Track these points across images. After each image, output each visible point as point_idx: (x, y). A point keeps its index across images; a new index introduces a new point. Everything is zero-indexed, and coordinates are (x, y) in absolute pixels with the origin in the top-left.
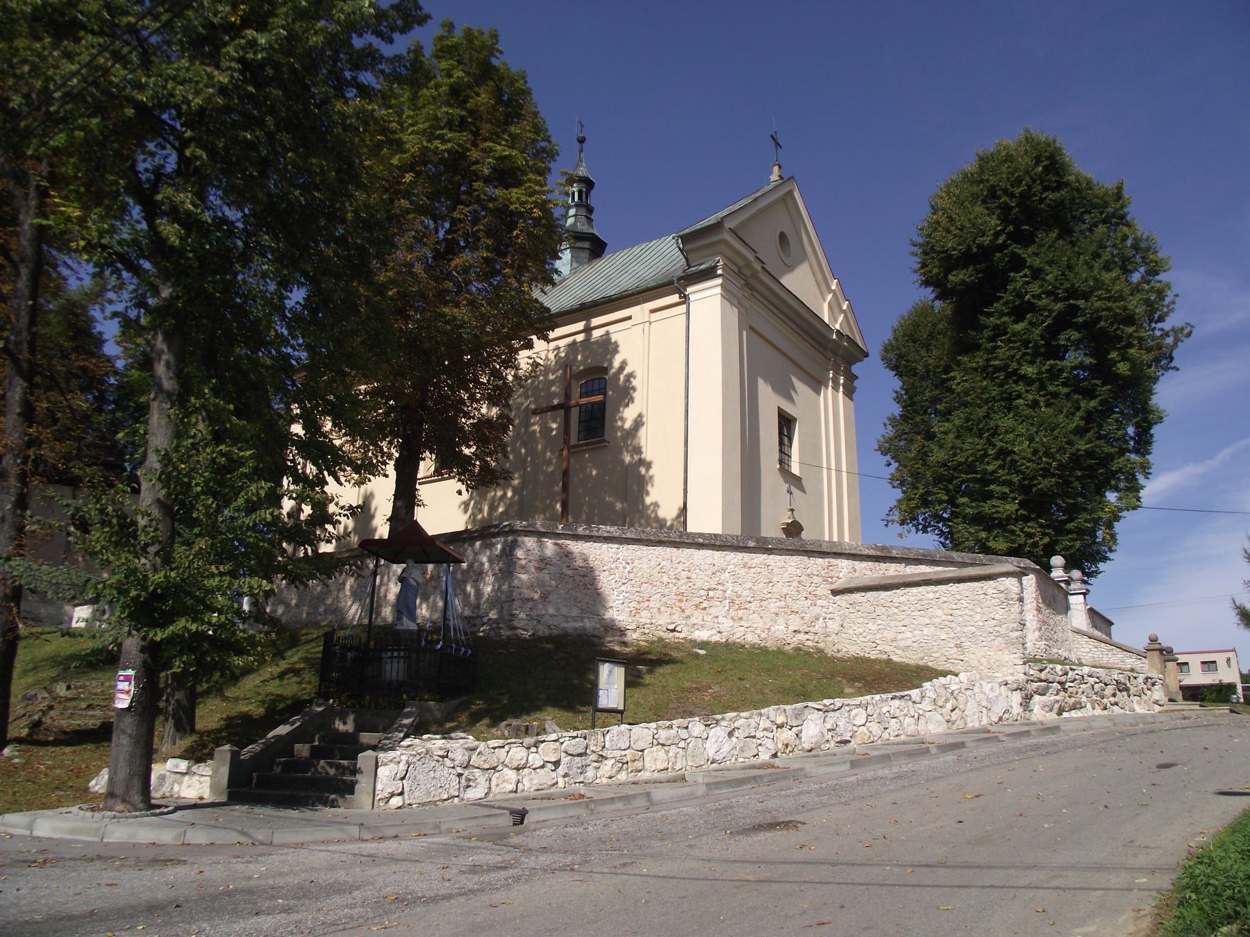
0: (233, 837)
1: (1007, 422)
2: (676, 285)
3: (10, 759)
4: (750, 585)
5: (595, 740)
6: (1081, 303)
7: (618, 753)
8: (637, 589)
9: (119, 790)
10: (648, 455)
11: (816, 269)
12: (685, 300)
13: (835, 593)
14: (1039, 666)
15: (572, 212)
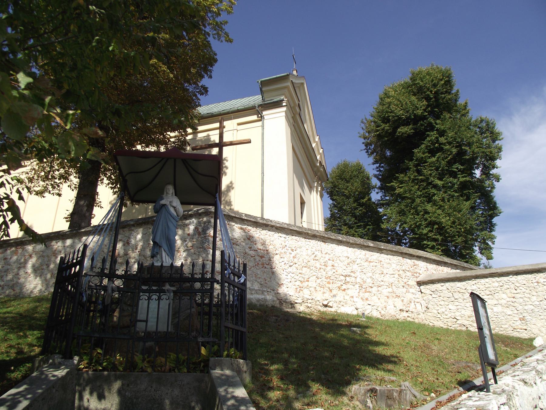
2: (257, 110)
4: (371, 274)
12: (261, 118)
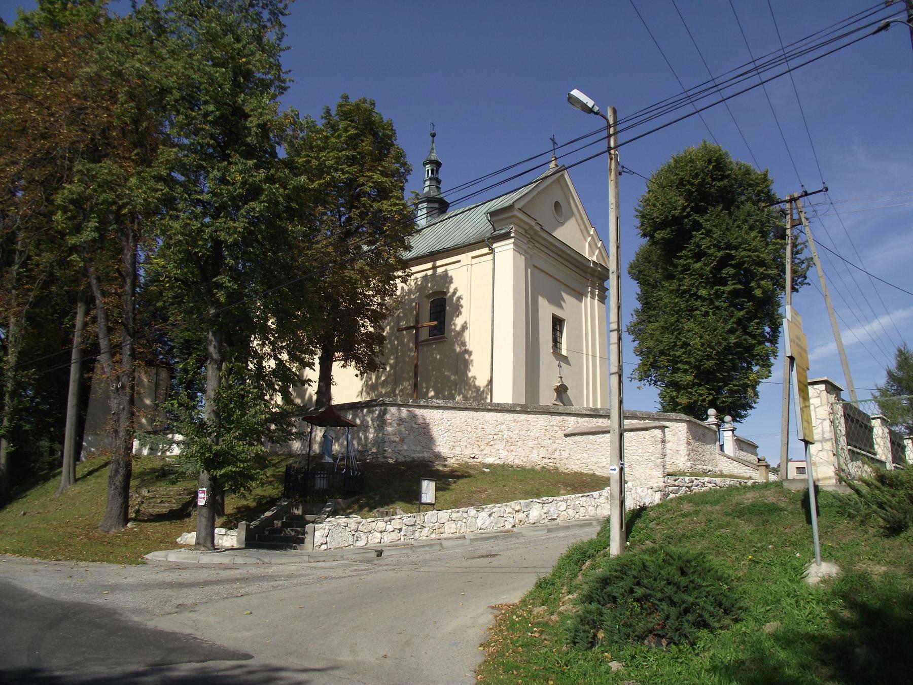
0: (254, 561)
1: (688, 325)
2: (487, 242)
3: (132, 529)
5: (419, 518)
6: (733, 252)
7: (431, 525)
8: (454, 435)
9: (201, 542)
10: (470, 346)
11: (580, 221)
12: (492, 251)
13: (566, 436)
14: (674, 478)
15: (427, 183)
